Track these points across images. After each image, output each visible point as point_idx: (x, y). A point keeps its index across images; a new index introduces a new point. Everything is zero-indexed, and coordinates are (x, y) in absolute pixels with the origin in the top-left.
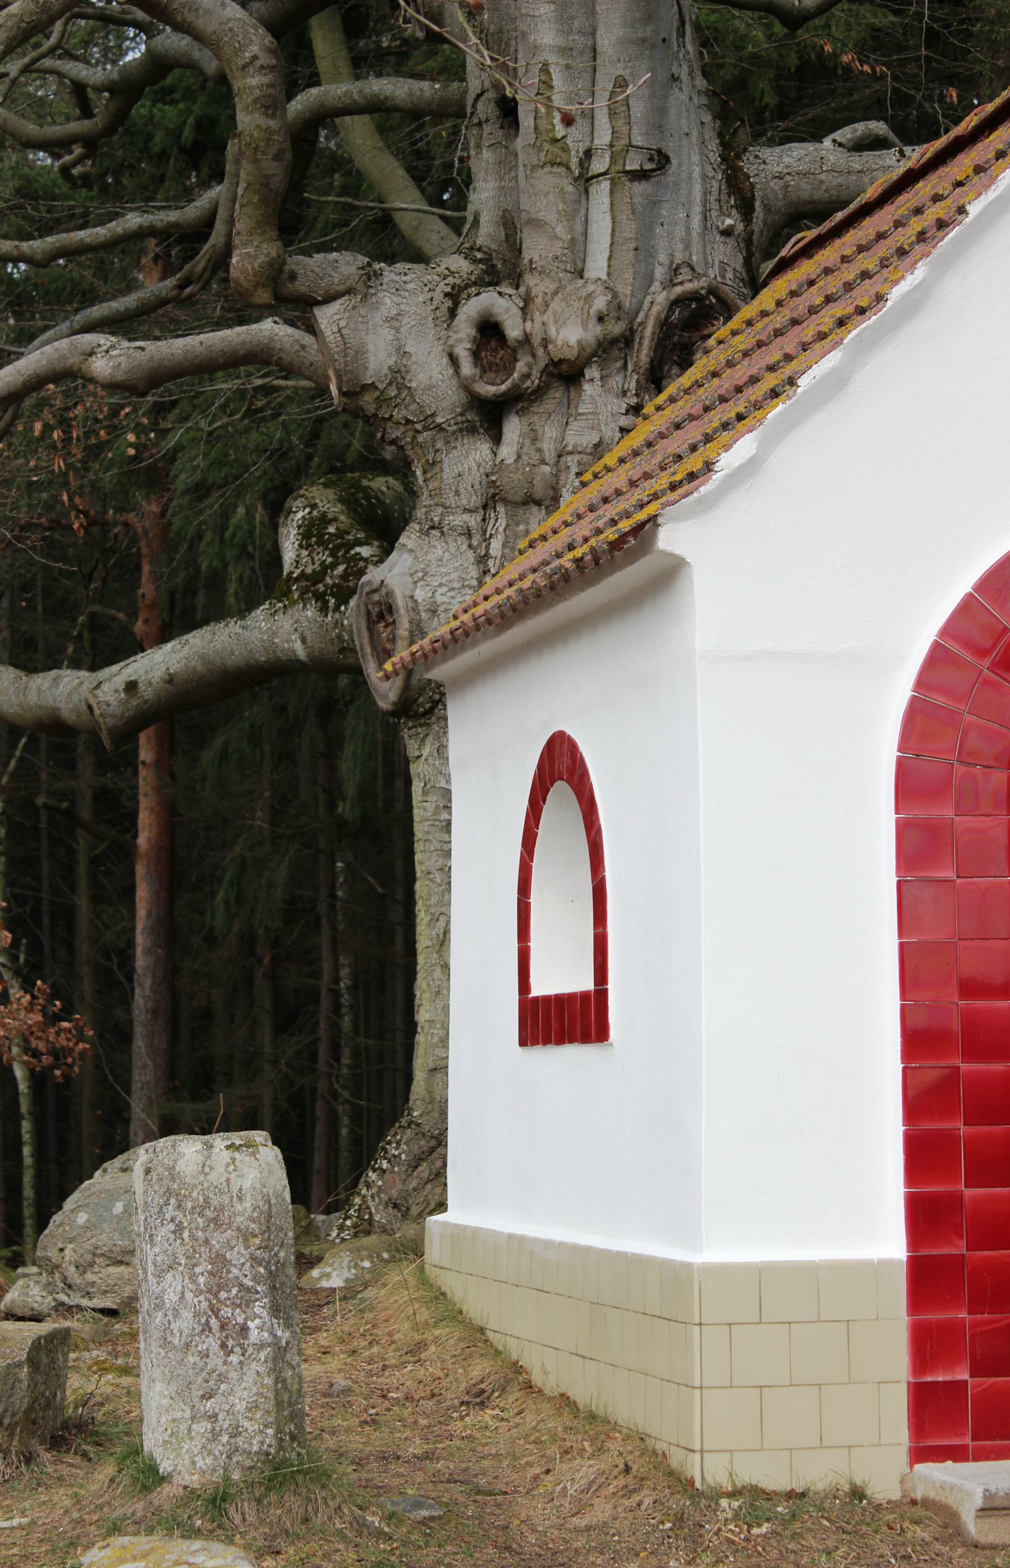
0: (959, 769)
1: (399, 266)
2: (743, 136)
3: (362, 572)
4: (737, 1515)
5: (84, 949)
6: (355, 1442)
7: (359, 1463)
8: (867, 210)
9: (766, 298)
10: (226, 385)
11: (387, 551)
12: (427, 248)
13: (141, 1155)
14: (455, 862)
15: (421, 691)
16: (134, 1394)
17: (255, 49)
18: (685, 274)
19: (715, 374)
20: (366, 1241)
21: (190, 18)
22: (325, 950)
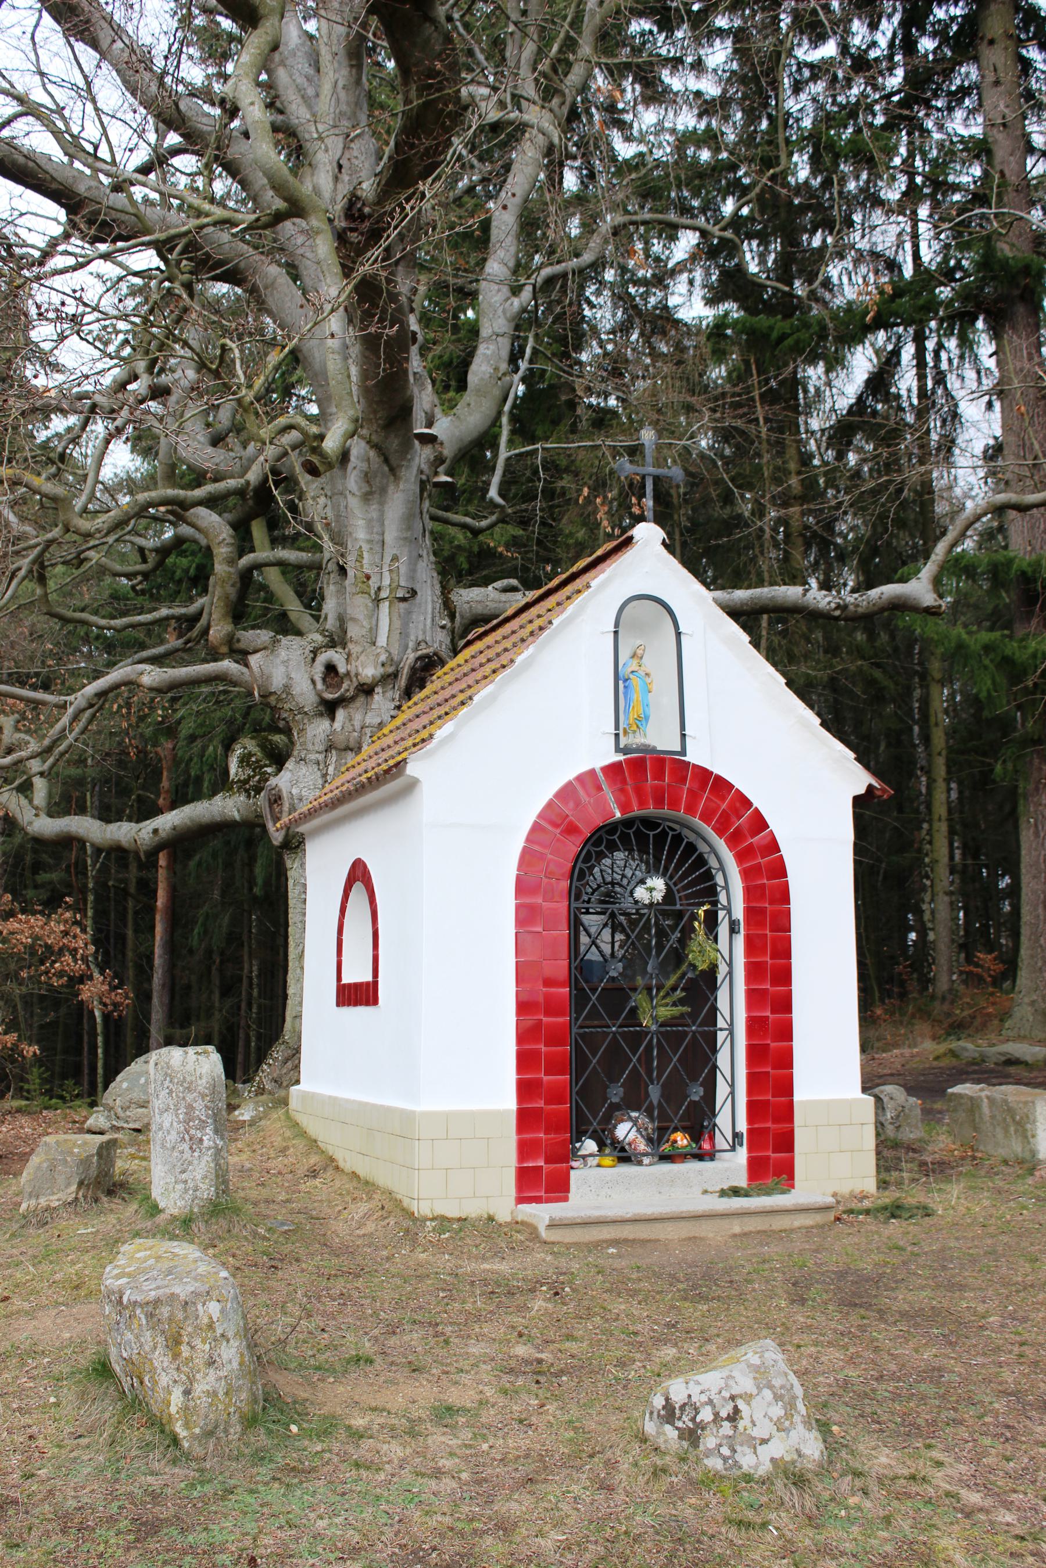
0: (545, 880)
1: (289, 637)
2: (453, 582)
3: (267, 780)
4: (434, 1229)
5: (130, 954)
6: (253, 1194)
7: (255, 1204)
8: (507, 620)
9: (460, 658)
10: (205, 689)
11: (279, 770)
12: (304, 630)
13: (154, 1056)
14: (307, 918)
15: (294, 837)
16: (148, 1170)
17: (224, 535)
18: (423, 645)
19: (436, 693)
20: (261, 1098)
21: (195, 520)
22: (246, 958)
